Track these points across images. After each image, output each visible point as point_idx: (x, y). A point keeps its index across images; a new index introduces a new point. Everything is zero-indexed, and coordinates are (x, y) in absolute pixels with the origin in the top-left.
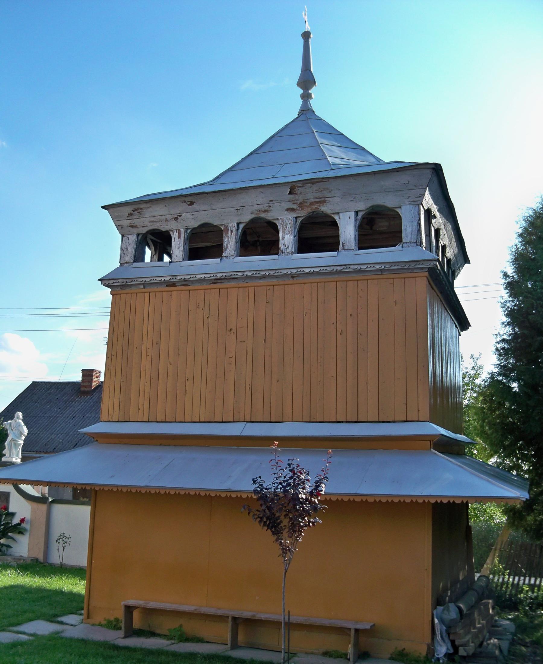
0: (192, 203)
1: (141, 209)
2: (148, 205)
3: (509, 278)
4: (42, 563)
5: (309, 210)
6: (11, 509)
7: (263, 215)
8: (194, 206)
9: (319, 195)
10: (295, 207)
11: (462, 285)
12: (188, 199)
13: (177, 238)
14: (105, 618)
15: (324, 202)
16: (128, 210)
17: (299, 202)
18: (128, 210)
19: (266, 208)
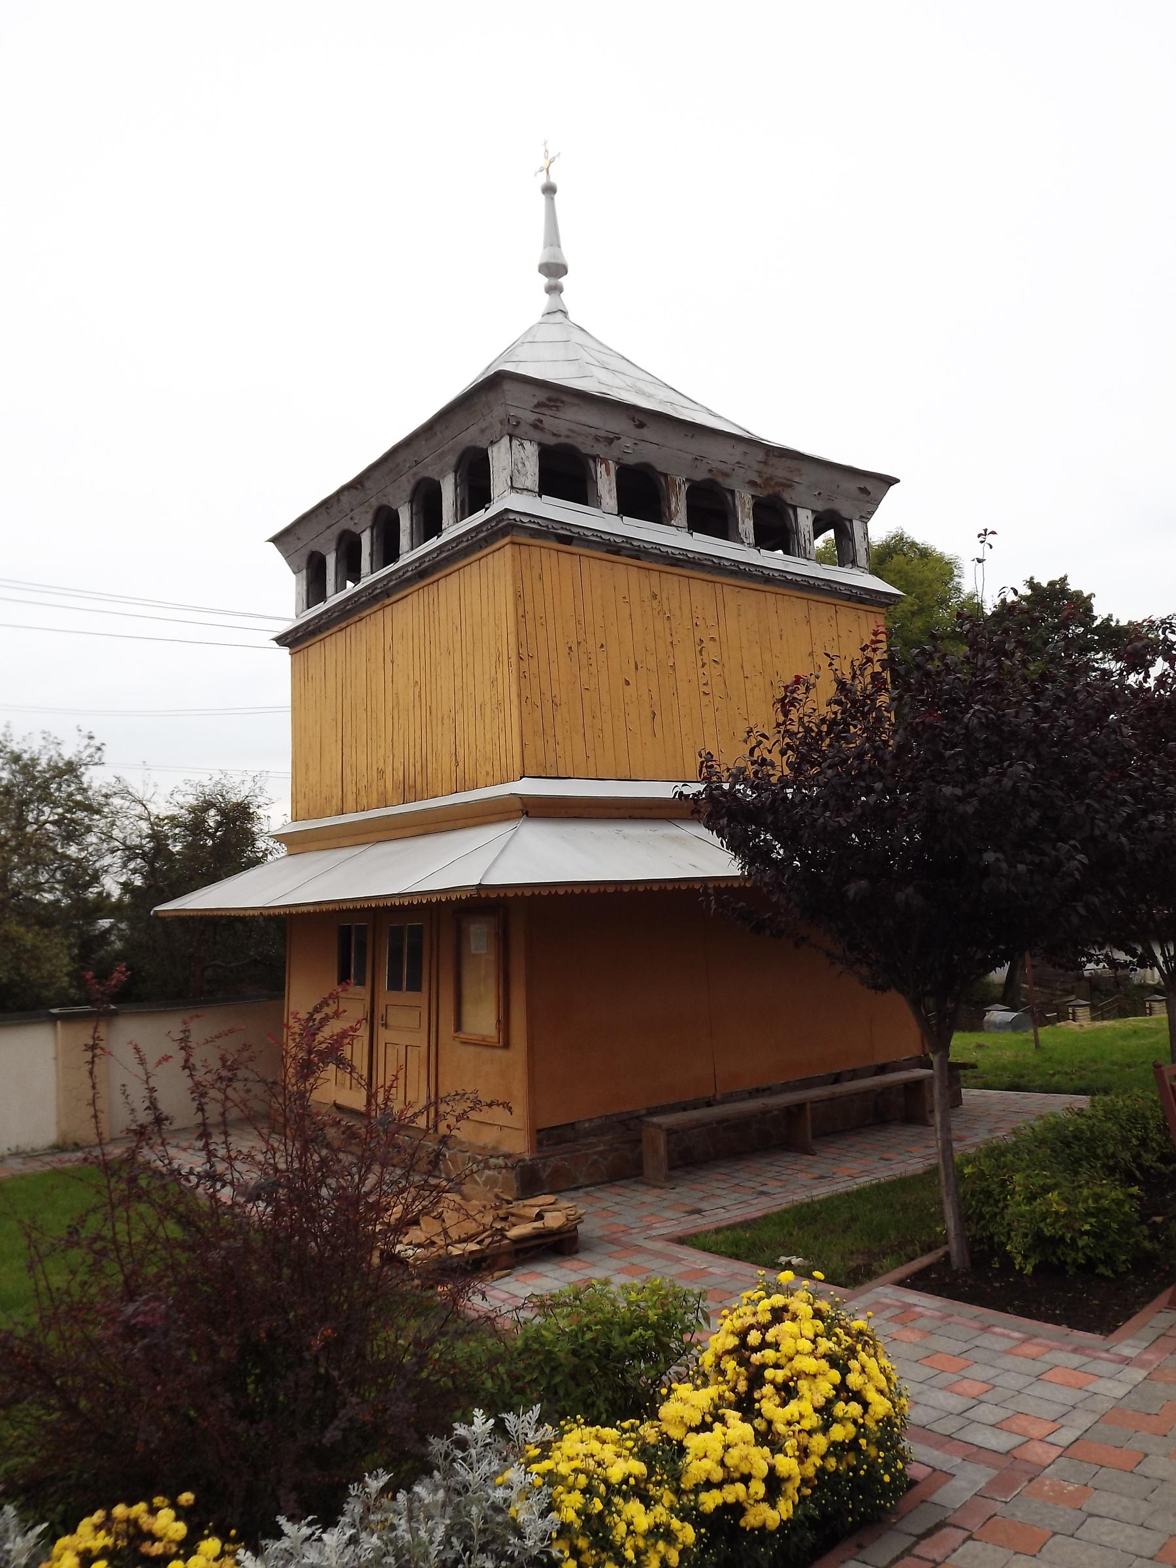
0: (641, 426)
1: (563, 402)
2: (576, 401)
3: (389, 1152)
4: (29, 951)
5: (771, 491)
6: (1095, 614)
7: (720, 479)
8: (644, 431)
9: (788, 476)
10: (759, 481)
11: (970, 1543)
12: (638, 417)
13: (604, 473)
14: (1032, 578)
15: (790, 486)
16: (542, 395)
17: (765, 476)
18: (542, 395)
19: (729, 471)
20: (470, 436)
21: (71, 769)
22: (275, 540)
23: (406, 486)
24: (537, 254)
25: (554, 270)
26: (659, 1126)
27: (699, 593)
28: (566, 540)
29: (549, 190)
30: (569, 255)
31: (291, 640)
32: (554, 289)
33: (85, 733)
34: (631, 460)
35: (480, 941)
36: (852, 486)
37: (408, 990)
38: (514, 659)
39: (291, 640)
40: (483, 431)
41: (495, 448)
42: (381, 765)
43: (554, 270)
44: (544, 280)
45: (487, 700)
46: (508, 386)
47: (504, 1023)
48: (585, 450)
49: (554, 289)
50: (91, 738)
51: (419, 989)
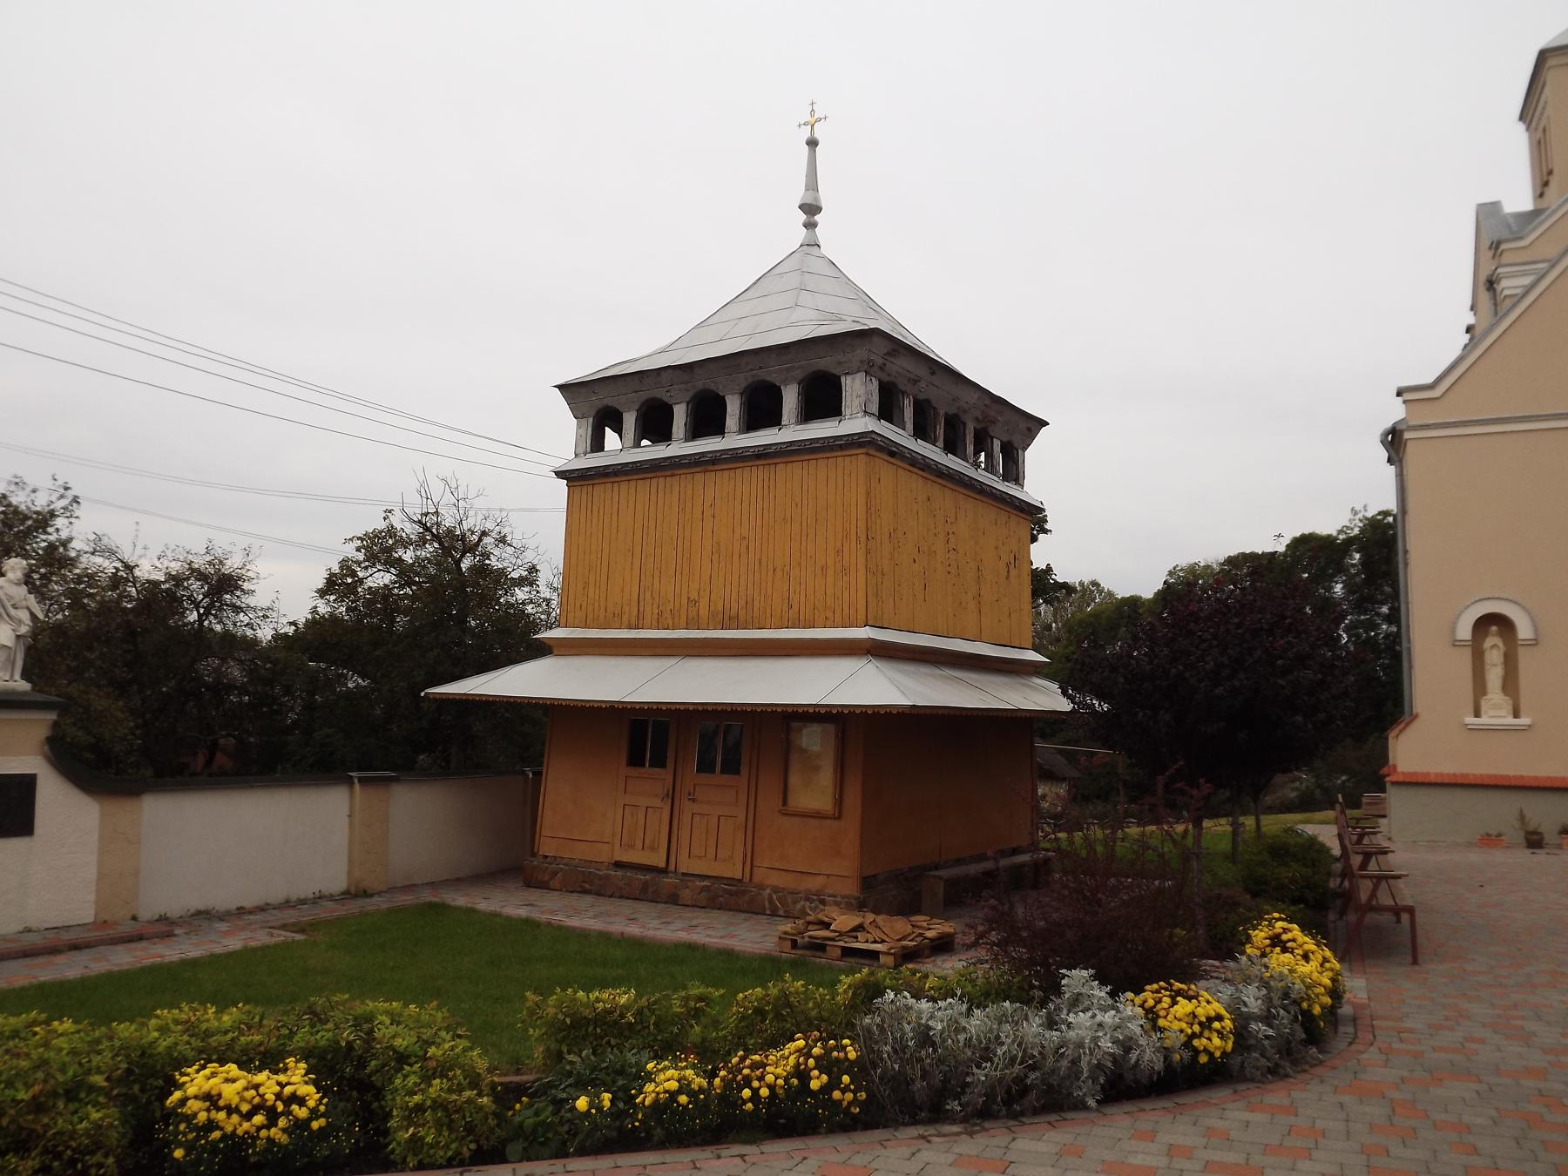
0: (933, 373)
20: (826, 363)
21: (44, 520)
22: (569, 390)
23: (743, 380)
24: (798, 194)
25: (811, 209)
26: (940, 878)
27: (945, 499)
28: (892, 454)
29: (812, 143)
30: (825, 200)
31: (572, 477)
32: (810, 226)
33: (60, 482)
34: (921, 397)
35: (812, 739)
36: (1023, 425)
37: (723, 772)
38: (863, 539)
39: (572, 477)
40: (840, 363)
41: (849, 378)
42: (694, 595)
43: (811, 209)
44: (803, 217)
45: (830, 561)
46: (876, 339)
47: (839, 802)
48: (902, 387)
49: (810, 226)
50: (66, 489)
51: (737, 772)
